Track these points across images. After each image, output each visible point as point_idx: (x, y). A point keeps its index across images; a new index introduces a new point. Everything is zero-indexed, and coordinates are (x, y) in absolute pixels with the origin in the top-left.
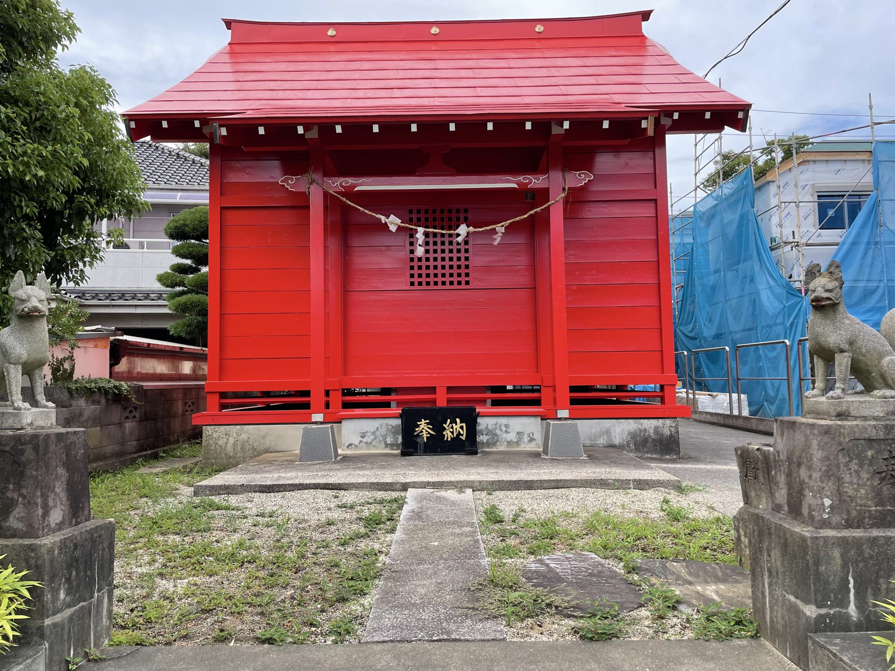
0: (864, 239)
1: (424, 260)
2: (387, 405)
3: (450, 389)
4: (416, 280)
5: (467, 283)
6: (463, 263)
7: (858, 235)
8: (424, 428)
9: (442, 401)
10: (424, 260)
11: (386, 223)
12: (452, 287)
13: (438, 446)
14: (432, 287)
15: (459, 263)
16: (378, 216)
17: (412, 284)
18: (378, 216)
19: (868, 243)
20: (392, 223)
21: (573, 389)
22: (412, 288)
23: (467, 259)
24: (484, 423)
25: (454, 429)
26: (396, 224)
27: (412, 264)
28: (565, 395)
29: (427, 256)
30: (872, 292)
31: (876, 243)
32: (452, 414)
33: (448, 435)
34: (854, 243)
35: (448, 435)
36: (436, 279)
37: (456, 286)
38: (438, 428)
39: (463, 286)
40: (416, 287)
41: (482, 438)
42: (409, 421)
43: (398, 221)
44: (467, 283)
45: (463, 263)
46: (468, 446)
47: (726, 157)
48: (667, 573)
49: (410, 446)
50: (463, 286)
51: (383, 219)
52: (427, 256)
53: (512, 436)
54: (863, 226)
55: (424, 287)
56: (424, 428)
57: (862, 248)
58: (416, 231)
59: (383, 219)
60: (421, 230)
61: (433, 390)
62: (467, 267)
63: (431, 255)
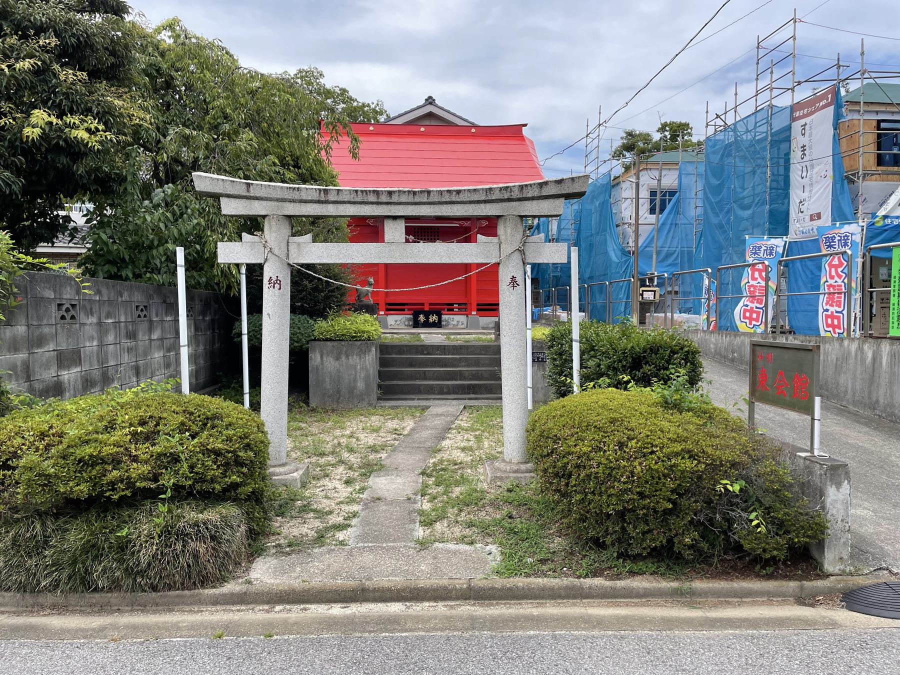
0: (669, 222)
2: (404, 310)
3: (430, 304)
7: (667, 218)
8: (422, 318)
9: (427, 308)
13: (427, 325)
19: (672, 224)
21: (478, 305)
24: (444, 317)
25: (433, 318)
28: (474, 306)
30: (672, 254)
31: (676, 224)
32: (432, 312)
33: (431, 320)
34: (663, 224)
35: (431, 320)
38: (427, 318)
41: (443, 323)
42: (416, 315)
46: (438, 325)
47: (630, 134)
48: (297, 177)
49: (416, 324)
53: (455, 323)
54: (670, 213)
56: (422, 318)
57: (668, 226)
61: (423, 304)
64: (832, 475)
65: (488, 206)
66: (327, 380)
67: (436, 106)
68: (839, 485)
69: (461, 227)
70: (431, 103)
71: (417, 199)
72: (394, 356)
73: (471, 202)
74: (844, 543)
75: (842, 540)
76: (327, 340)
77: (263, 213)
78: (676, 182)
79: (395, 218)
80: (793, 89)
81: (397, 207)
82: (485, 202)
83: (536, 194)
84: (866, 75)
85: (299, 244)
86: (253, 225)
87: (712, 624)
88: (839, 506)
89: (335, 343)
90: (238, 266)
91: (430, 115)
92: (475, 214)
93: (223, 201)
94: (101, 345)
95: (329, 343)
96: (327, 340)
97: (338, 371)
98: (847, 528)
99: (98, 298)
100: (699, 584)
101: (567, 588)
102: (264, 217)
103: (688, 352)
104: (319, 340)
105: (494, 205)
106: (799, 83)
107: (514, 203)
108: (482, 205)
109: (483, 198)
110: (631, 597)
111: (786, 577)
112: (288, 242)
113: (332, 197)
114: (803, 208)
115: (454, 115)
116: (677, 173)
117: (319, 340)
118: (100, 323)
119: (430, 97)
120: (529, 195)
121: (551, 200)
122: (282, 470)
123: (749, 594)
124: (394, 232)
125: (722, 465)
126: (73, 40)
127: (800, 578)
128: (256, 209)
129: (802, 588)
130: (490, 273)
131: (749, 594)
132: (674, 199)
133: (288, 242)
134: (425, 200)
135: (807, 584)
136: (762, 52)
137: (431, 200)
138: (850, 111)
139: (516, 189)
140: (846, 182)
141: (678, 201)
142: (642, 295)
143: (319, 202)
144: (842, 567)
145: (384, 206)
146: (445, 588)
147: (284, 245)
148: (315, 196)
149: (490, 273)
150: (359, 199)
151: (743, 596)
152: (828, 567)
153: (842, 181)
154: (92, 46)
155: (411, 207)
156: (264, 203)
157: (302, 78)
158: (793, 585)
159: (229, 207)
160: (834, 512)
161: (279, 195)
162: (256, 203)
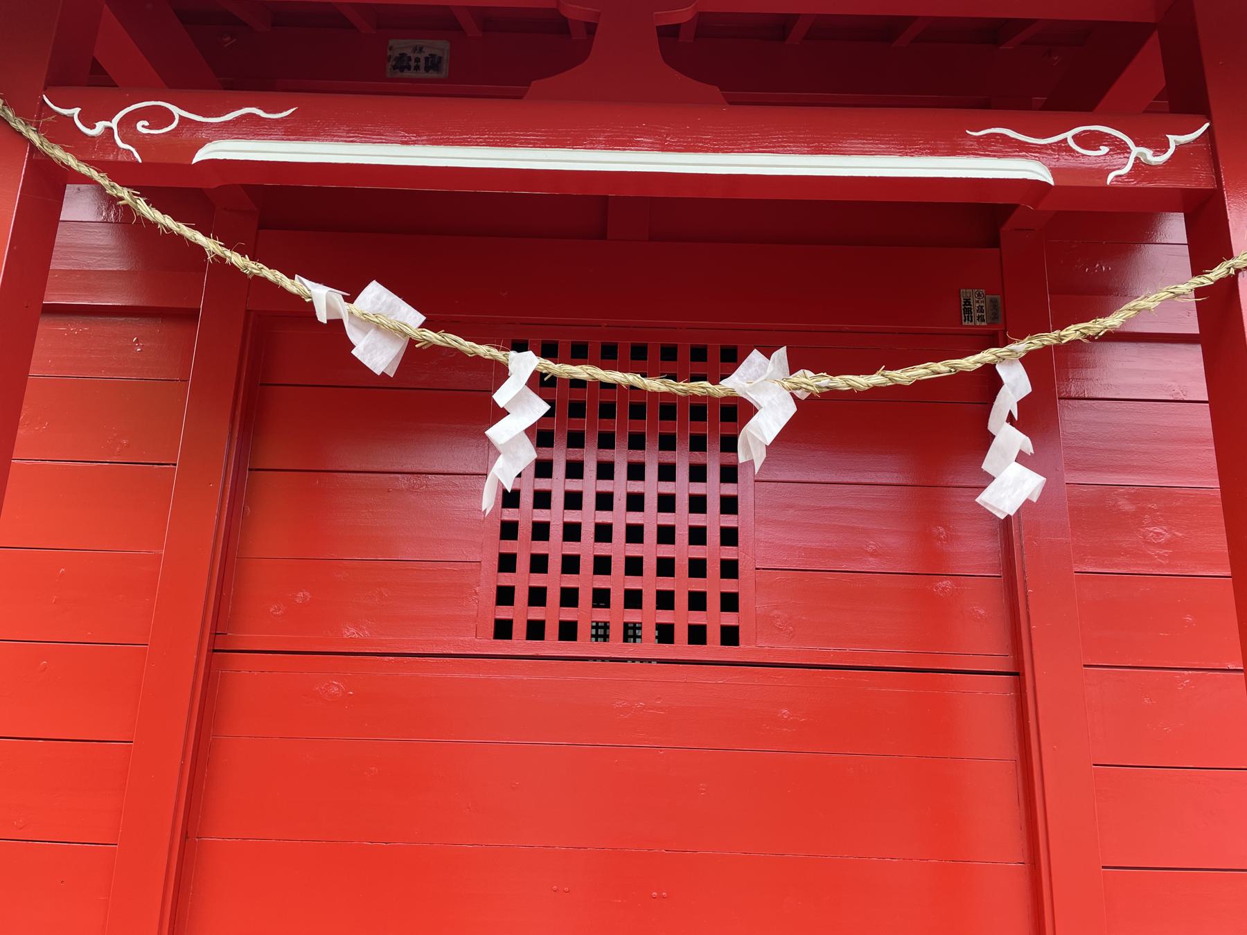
1: (527, 499)
4: (520, 613)
5: (730, 636)
6: (713, 551)
10: (527, 499)
11: (336, 325)
12: (697, 652)
14: (615, 646)
15: (697, 552)
16: (299, 285)
17: (503, 630)
18: (299, 285)
20: (367, 323)
22: (503, 647)
23: (729, 537)
26: (393, 332)
27: (509, 547)
29: (543, 484)
36: (553, 596)
37: (681, 648)
39: (713, 649)
40: (519, 644)
43: (410, 318)
44: (730, 636)
45: (713, 551)
50: (713, 649)
51: (324, 299)
52: (543, 484)
55: (551, 645)
58: (501, 373)
59: (324, 299)
60: (524, 364)
62: (730, 569)
63: (558, 485)
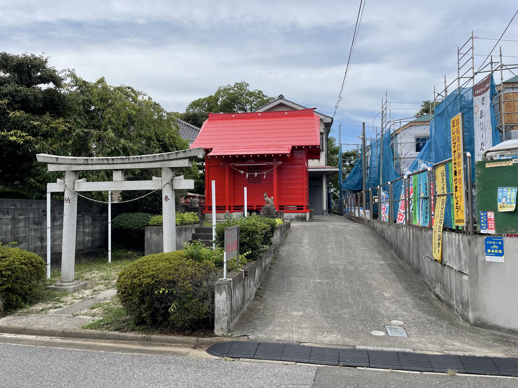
3: (257, 206)
19: (426, 157)
31: (429, 157)
47: (427, 103)
54: (425, 151)
61: (253, 206)
64: (218, 288)
65: (155, 163)
66: (153, 245)
67: (284, 100)
68: (221, 293)
69: (268, 165)
70: (281, 98)
71: (124, 162)
72: (202, 234)
73: (147, 162)
74: (224, 321)
75: (223, 320)
76: (154, 225)
77: (64, 170)
78: (429, 132)
79: (117, 170)
80: (473, 78)
81: (117, 165)
82: (154, 162)
83: (175, 157)
84: (504, 68)
85: (78, 183)
86: (60, 175)
87: (151, 352)
88: (221, 303)
89: (157, 227)
90: (107, 192)
91: (281, 105)
92: (150, 167)
93: (49, 165)
94: (14, 227)
95: (154, 227)
96: (154, 225)
97: (158, 241)
98: (225, 314)
99: (13, 207)
100: (154, 336)
101: (100, 334)
102: (65, 172)
103: (250, 231)
104: (150, 225)
105: (158, 163)
106: (476, 74)
107: (166, 162)
108: (153, 163)
109: (152, 160)
110: (125, 340)
111: (190, 335)
112: (74, 182)
113: (90, 162)
114: (484, 147)
115: (294, 103)
116: (429, 127)
117: (150, 225)
118: (14, 218)
119: (281, 95)
120: (172, 158)
121: (183, 160)
122: (67, 284)
123: (175, 342)
124: (117, 176)
125: (163, 282)
126: (19, 98)
127: (198, 336)
128: (62, 168)
129: (197, 340)
130: (157, 195)
131: (175, 342)
132: (428, 142)
133: (74, 182)
134: (128, 162)
135: (200, 339)
136: (460, 56)
137: (130, 162)
138: (505, 88)
139: (166, 156)
140: (498, 131)
141: (430, 144)
142: (374, 200)
143: (85, 164)
144: (223, 333)
145: (112, 165)
146: (54, 331)
147: (72, 183)
148: (83, 162)
149: (157, 195)
150: (100, 162)
151: (171, 343)
152: (216, 332)
153: (496, 130)
154: (28, 100)
155: (122, 165)
156: (64, 166)
157: (237, 87)
158: (193, 339)
159: (51, 168)
160: (219, 306)
161: (69, 162)
162: (61, 166)
